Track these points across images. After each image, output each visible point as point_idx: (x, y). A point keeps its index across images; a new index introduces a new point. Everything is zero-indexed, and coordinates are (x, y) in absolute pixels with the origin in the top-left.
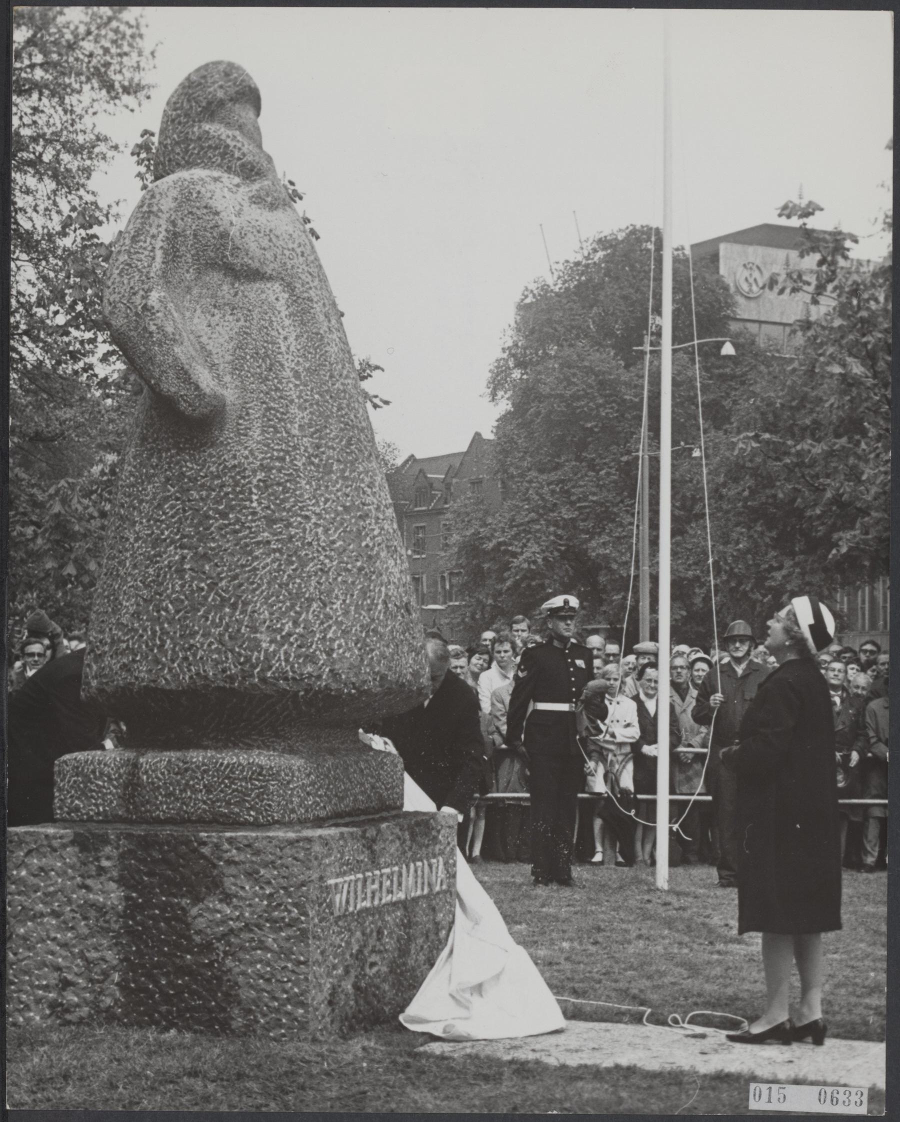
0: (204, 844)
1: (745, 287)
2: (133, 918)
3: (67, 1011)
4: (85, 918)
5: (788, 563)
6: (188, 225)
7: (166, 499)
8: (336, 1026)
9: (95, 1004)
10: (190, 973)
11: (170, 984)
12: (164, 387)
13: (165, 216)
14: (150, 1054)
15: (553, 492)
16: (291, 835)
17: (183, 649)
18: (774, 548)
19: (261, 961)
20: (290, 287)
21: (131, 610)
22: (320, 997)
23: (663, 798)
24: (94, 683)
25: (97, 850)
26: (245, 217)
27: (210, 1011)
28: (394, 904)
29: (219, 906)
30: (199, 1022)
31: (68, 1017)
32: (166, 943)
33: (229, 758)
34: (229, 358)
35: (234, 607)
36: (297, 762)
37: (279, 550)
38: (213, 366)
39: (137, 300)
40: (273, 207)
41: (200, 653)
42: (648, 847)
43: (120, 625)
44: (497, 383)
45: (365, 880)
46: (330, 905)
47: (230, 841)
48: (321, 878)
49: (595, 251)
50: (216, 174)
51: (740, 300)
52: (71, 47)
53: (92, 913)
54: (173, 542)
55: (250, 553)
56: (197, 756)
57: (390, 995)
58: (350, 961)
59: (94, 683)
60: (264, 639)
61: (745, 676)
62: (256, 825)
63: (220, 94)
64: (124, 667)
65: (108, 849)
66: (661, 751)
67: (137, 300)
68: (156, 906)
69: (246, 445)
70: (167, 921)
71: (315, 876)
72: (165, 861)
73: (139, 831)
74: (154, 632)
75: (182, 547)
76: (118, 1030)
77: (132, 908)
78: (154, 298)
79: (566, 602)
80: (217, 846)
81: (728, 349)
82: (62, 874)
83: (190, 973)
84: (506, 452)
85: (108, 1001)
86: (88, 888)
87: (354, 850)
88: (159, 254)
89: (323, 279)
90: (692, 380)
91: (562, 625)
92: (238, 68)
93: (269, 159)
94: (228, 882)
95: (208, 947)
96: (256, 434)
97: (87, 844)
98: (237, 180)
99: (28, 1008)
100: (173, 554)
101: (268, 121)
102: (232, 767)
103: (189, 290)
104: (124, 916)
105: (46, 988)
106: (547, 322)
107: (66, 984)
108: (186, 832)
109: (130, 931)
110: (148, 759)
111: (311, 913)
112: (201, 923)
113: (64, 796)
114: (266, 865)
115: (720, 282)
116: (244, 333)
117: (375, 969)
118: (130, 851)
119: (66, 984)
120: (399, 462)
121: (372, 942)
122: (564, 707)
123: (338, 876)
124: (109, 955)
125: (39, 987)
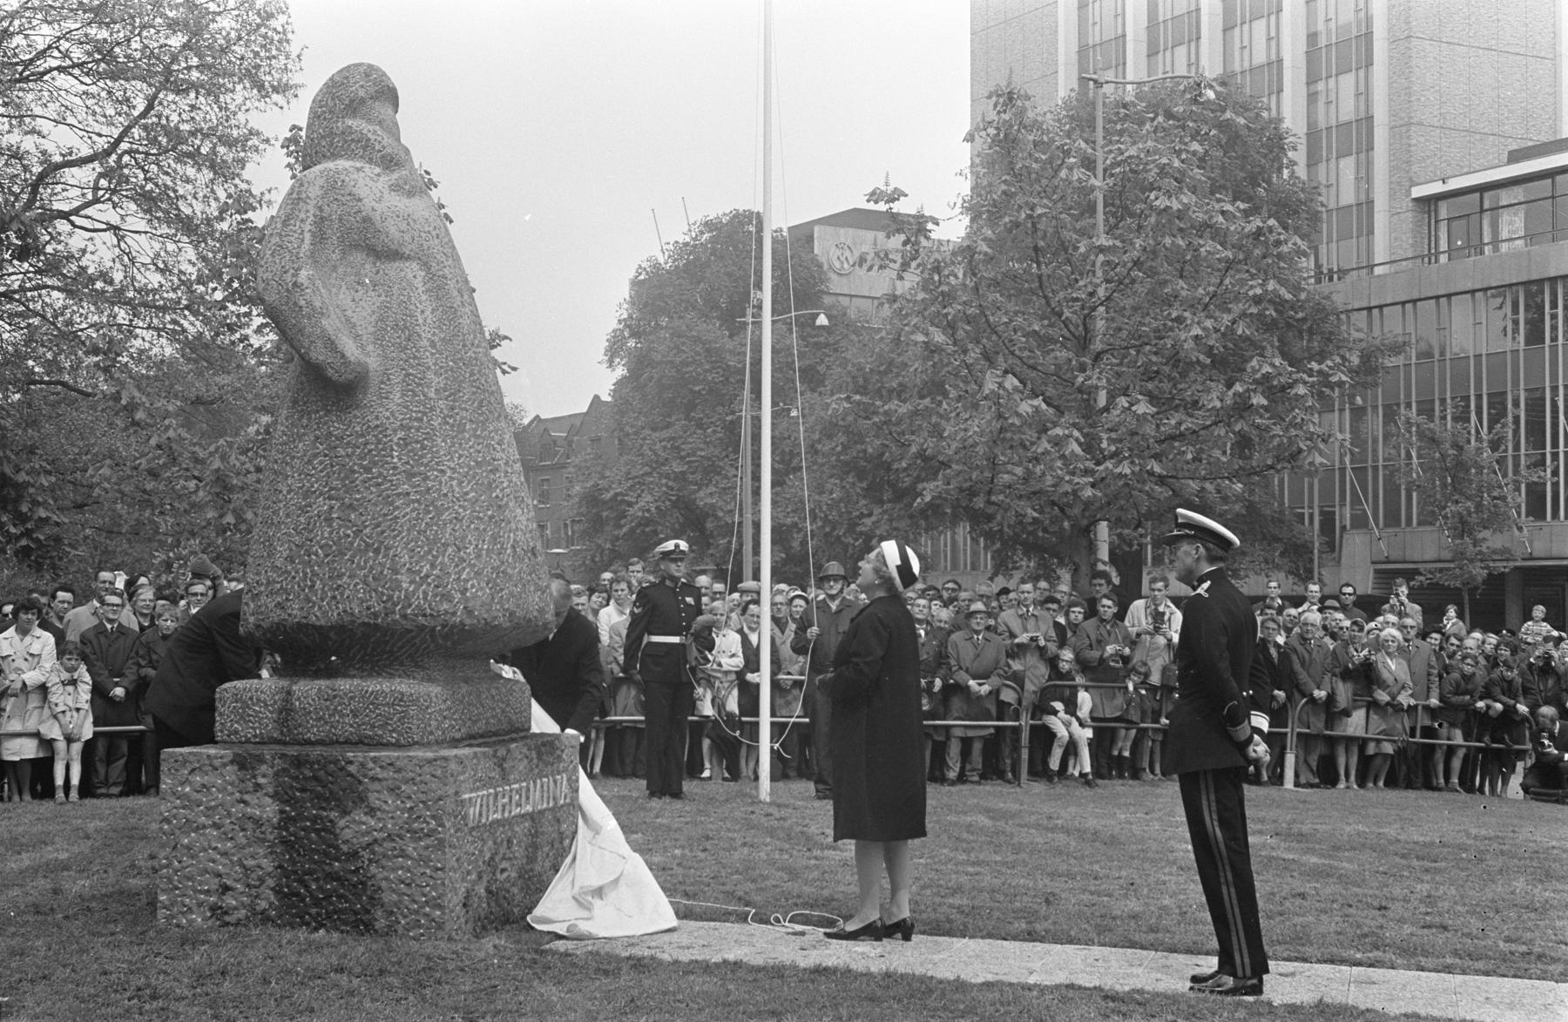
0: (351, 762)
1: (837, 265)
2: (287, 830)
3: (226, 913)
4: (243, 830)
5: (877, 511)
6: (334, 211)
7: (315, 456)
8: (470, 926)
9: (252, 908)
10: (338, 879)
11: (320, 888)
12: (313, 355)
14: (300, 953)
16: (430, 755)
17: (331, 589)
18: (864, 497)
20: (426, 266)
22: (455, 900)
24: (252, 619)
27: (356, 913)
29: (364, 819)
31: (227, 918)
32: (317, 851)
33: (374, 685)
34: (372, 329)
36: (435, 689)
37: (418, 501)
39: (288, 277)
40: (410, 194)
41: (347, 593)
42: (752, 765)
44: (614, 350)
45: (496, 795)
46: (465, 817)
47: (374, 760)
48: (457, 793)
49: (702, 233)
50: (358, 165)
51: (833, 276)
52: (223, 51)
53: (250, 825)
55: (391, 504)
56: (344, 684)
58: (483, 868)
59: (252, 619)
60: (404, 580)
61: (839, 612)
62: (398, 746)
63: (361, 93)
65: (264, 768)
66: (763, 678)
67: (288, 277)
68: (307, 819)
69: (388, 406)
70: (317, 831)
71: (451, 791)
72: (315, 778)
73: (292, 751)
74: (305, 574)
75: (330, 498)
76: (272, 931)
77: (286, 821)
79: (677, 546)
80: (362, 765)
81: (822, 320)
82: (222, 790)
83: (338, 879)
84: (622, 413)
85: (263, 904)
86: (244, 802)
87: (486, 767)
88: (307, 236)
89: (457, 259)
90: (790, 348)
91: (673, 567)
92: (378, 70)
93: (407, 151)
94: (372, 797)
95: (354, 855)
96: (396, 397)
97: (242, 763)
98: (378, 170)
99: (190, 910)
101: (404, 117)
102: (375, 694)
103: (335, 268)
104: (279, 827)
105: (207, 892)
106: (656, 295)
107: (226, 889)
108: (335, 752)
109: (284, 842)
111: (448, 825)
113: (224, 720)
114: (406, 782)
116: (386, 307)
117: (505, 875)
118: (284, 770)
119: (226, 889)
120: (526, 421)
121: (502, 850)
122: (676, 640)
123: (472, 791)
124: (265, 862)
125: (201, 892)
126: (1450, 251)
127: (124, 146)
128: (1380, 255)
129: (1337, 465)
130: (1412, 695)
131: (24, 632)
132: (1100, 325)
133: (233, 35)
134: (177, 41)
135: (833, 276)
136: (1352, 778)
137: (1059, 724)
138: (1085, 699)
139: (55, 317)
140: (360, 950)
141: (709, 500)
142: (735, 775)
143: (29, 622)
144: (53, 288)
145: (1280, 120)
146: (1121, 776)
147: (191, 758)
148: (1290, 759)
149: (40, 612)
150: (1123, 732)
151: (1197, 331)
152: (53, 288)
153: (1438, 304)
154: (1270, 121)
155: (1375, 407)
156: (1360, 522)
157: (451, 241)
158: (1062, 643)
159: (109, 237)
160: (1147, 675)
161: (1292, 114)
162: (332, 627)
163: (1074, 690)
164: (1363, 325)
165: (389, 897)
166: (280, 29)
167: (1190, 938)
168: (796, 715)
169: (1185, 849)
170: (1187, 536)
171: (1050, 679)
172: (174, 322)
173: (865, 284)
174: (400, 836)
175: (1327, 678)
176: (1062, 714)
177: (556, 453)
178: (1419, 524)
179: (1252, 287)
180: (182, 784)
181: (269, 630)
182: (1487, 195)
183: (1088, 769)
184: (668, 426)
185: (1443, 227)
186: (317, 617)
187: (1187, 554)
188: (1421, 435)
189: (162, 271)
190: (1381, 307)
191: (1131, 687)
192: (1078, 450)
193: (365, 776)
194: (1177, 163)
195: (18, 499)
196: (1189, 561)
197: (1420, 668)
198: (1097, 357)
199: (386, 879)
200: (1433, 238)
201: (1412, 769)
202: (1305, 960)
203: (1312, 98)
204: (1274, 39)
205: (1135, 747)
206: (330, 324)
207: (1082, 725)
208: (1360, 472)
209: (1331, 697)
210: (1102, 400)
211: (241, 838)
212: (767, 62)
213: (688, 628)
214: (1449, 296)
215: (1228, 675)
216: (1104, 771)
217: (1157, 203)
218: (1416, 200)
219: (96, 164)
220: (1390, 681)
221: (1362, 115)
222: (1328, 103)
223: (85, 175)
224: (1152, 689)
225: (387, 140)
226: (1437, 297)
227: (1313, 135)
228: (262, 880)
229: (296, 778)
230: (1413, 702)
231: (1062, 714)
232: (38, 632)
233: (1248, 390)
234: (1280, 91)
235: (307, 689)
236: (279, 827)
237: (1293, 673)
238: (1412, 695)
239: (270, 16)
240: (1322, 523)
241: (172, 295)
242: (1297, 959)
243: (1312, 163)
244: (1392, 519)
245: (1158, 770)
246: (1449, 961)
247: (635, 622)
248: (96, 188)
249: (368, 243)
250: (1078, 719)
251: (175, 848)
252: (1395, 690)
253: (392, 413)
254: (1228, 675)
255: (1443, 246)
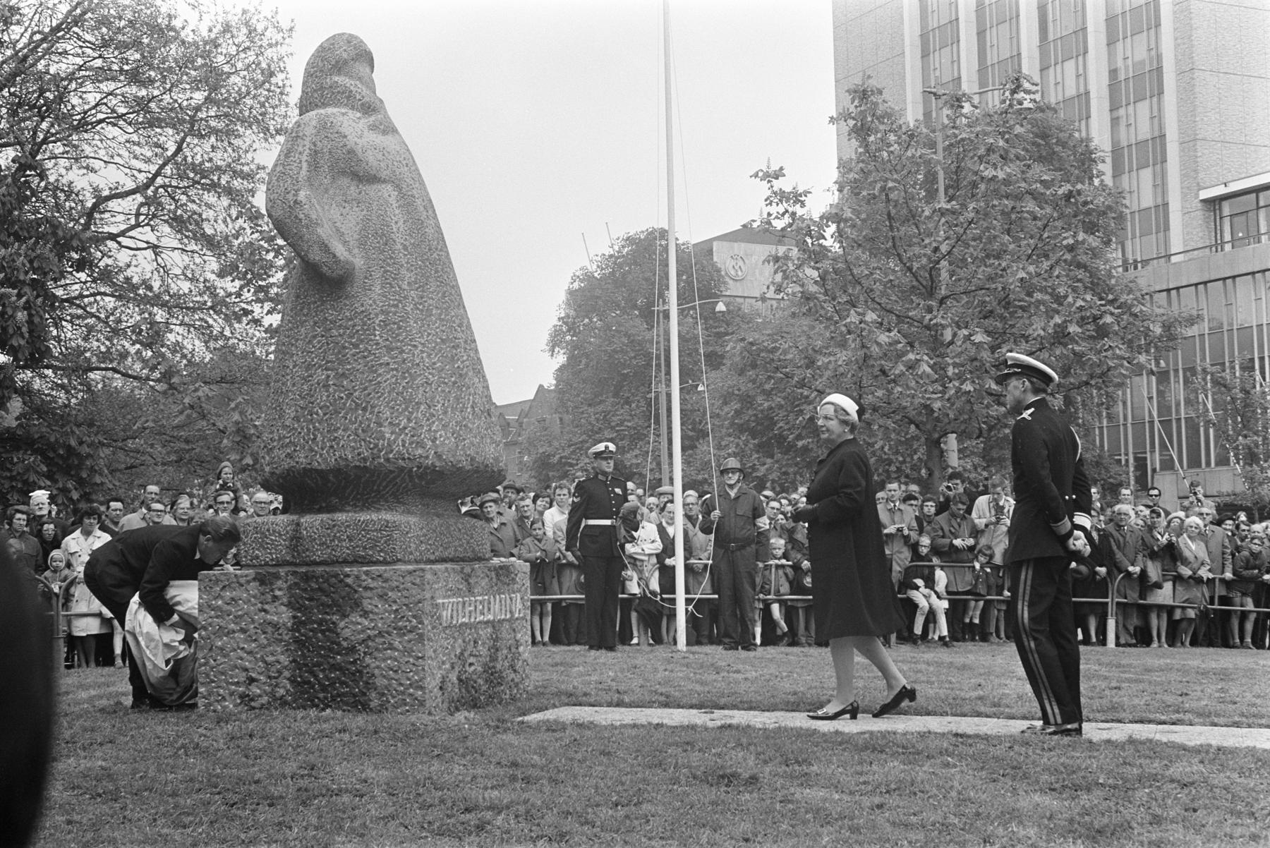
0: (348, 576)
1: (733, 272)
2: (299, 631)
3: (252, 700)
4: (265, 633)
5: (769, 461)
6: (325, 146)
7: (315, 337)
8: (446, 705)
9: (272, 694)
10: (341, 669)
12: (311, 256)
13: (308, 139)
15: (597, 420)
16: (410, 567)
17: (330, 440)
18: (758, 452)
19: (390, 658)
20: (398, 187)
21: (292, 415)
22: (434, 683)
23: (681, 595)
24: (267, 469)
25: (271, 584)
26: (364, 140)
27: (355, 696)
28: (488, 622)
29: (359, 620)
30: (347, 704)
31: (253, 704)
33: (364, 516)
34: (356, 236)
35: (365, 409)
36: (413, 520)
37: (396, 369)
38: (345, 243)
39: (290, 197)
40: (385, 133)
41: (342, 443)
42: (672, 634)
43: (285, 427)
45: (464, 603)
46: (439, 618)
47: (367, 573)
48: (432, 598)
49: (623, 247)
50: (343, 111)
53: (270, 629)
54: (320, 366)
55: (376, 371)
56: (341, 517)
57: (484, 688)
58: (455, 660)
59: (267, 469)
60: (387, 431)
61: (737, 498)
62: (385, 563)
63: (345, 55)
64: (288, 455)
66: (678, 561)
67: (290, 197)
68: (315, 622)
69: (371, 297)
70: (323, 632)
71: (428, 596)
72: (320, 589)
74: (309, 430)
75: (327, 369)
77: (298, 624)
78: (302, 195)
79: (607, 447)
80: (357, 577)
81: (721, 307)
82: (248, 602)
83: (341, 669)
85: (282, 691)
86: (265, 611)
87: (455, 581)
88: (305, 165)
89: (422, 183)
90: (696, 337)
91: (604, 463)
92: (356, 38)
93: (381, 101)
94: (365, 602)
95: (352, 649)
96: (378, 289)
98: (359, 115)
99: (224, 699)
100: (320, 375)
102: (366, 522)
103: (326, 191)
104: (292, 630)
105: (237, 684)
106: (589, 299)
107: (252, 680)
108: (337, 569)
109: (297, 641)
110: (307, 520)
111: (426, 622)
112: (347, 633)
114: (393, 590)
115: (713, 265)
116: (367, 219)
117: (473, 668)
118: (296, 584)
119: (252, 680)
121: (470, 648)
122: (608, 522)
123: (444, 597)
124: (282, 658)
125: (232, 684)
126: (1233, 241)
127: (159, 181)
128: (1176, 244)
129: (1147, 419)
130: (1210, 570)
131: (87, 533)
132: (944, 275)
133: (244, 89)
134: (199, 96)
135: (731, 282)
136: (1163, 639)
137: (920, 596)
138: (941, 577)
139: (107, 317)
140: (360, 721)
141: (634, 461)
142: (658, 640)
143: (91, 524)
144: (105, 294)
145: (1089, 139)
146: (973, 640)
147: (223, 578)
148: (1111, 624)
149: (100, 517)
150: (973, 603)
151: (1022, 274)
152: (105, 294)
153: (1225, 285)
154: (1082, 141)
155: (1176, 371)
156: (1168, 465)
157: (417, 169)
158: (921, 531)
159: (149, 254)
160: (991, 557)
161: (1099, 134)
162: (331, 471)
163: (932, 569)
164: (1164, 302)
165: (381, 682)
166: (280, 84)
167: (1024, 710)
168: (704, 592)
169: (1021, 671)
170: (1015, 374)
171: (912, 561)
172: (201, 319)
173: (751, 279)
174: (388, 633)
175: (1140, 557)
176: (922, 589)
177: (510, 433)
178: (1217, 465)
179: (1065, 238)
180: (215, 598)
181: (280, 476)
182: (1261, 195)
183: (945, 633)
184: (601, 402)
185: (1227, 222)
186: (318, 463)
187: (1016, 387)
188: (1216, 382)
189: (191, 280)
190: (1177, 289)
191: (977, 566)
192: (928, 370)
193: (360, 586)
194: (1001, 143)
195: (79, 467)
196: (1017, 393)
197: (1217, 551)
198: (942, 302)
199: (378, 667)
200: (1218, 231)
201: (1214, 630)
202: (1120, 721)
203: (1115, 122)
204: (1082, 76)
205: (984, 615)
206: (324, 232)
207: (939, 597)
208: (1166, 424)
209: (1144, 572)
210: (948, 335)
211: (263, 639)
212: (667, 81)
213: (617, 513)
214: (1234, 277)
215: (1049, 481)
216: (960, 636)
217: (986, 173)
218: (1203, 201)
219: (138, 195)
220: (1192, 559)
221: (1156, 134)
222: (1129, 125)
223: (131, 204)
224: (996, 568)
225: (365, 91)
226: (1224, 279)
227: (1117, 152)
228: (280, 672)
229: (305, 590)
230: (1211, 576)
231: (922, 589)
232: (99, 533)
233: (1065, 321)
234: (1088, 117)
235: (312, 522)
236: (292, 630)
237: (1112, 553)
238: (1210, 570)
239: (272, 74)
240: (1136, 468)
241: (198, 299)
242: (1113, 721)
243: (1117, 172)
244: (1194, 462)
245: (1003, 635)
246: (1237, 719)
247: (575, 510)
248: (138, 215)
249: (352, 170)
250: (936, 593)
251: (211, 649)
252: (1195, 566)
253: (374, 302)
254: (1049, 481)
255: (1227, 237)
